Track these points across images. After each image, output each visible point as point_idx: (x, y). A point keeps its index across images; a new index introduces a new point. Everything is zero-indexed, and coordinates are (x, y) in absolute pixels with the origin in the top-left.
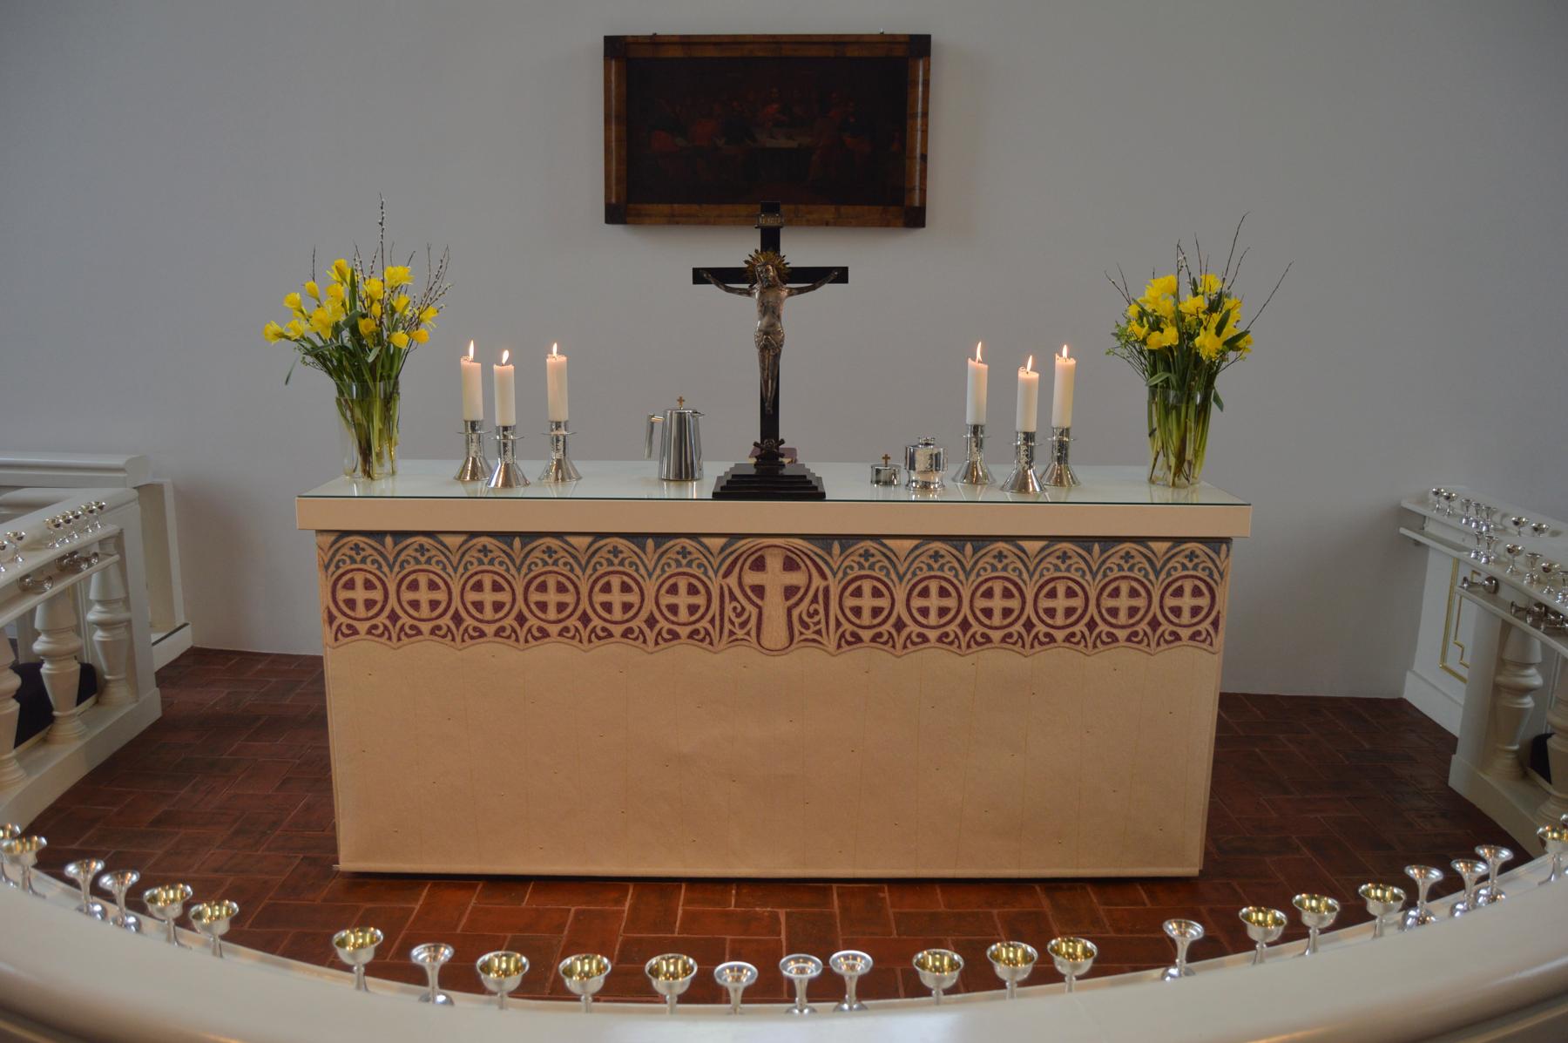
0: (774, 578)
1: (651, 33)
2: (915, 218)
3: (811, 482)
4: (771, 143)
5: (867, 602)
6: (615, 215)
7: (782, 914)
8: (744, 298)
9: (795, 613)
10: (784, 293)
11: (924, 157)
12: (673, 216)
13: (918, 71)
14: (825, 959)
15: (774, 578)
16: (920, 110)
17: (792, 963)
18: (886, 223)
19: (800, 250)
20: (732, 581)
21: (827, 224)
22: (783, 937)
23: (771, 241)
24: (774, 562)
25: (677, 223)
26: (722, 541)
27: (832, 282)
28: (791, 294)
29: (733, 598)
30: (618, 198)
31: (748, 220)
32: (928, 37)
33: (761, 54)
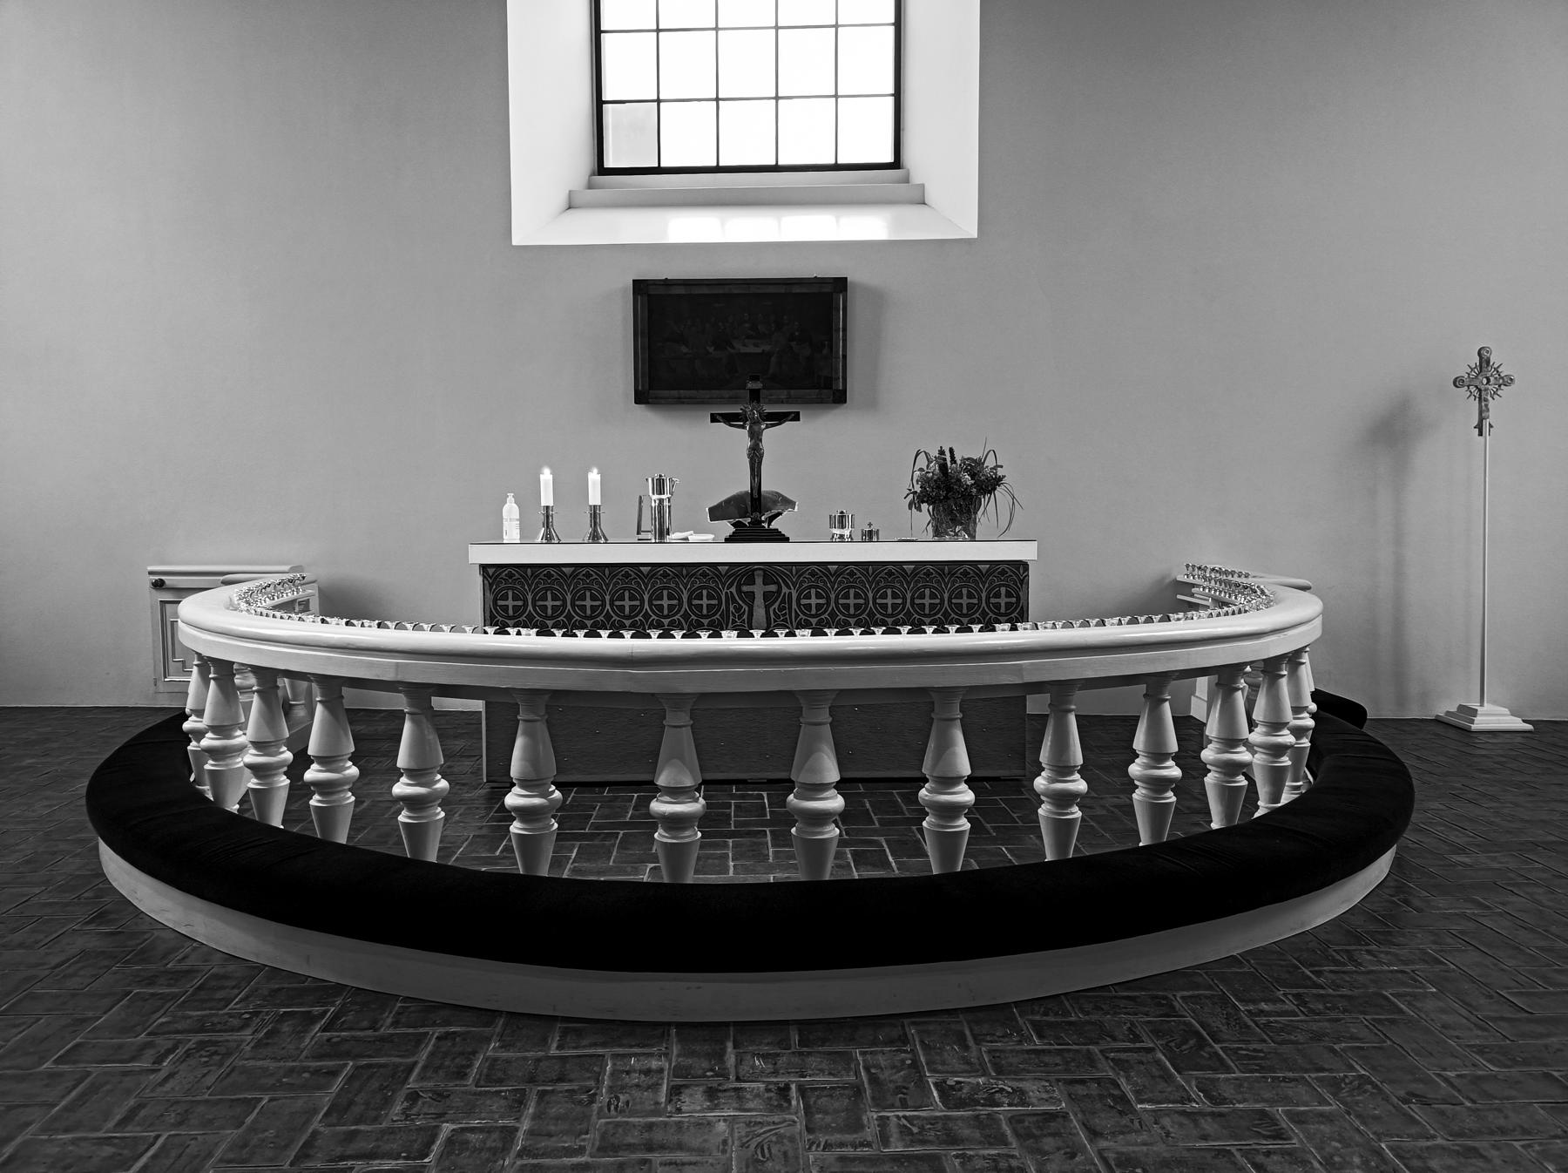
0: (758, 589)
4: (744, 350)
6: (640, 398)
7: (765, 794)
9: (771, 609)
10: (763, 427)
11: (845, 357)
12: (679, 398)
15: (758, 589)
16: (841, 326)
20: (733, 590)
21: (782, 402)
22: (766, 801)
24: (759, 580)
25: (683, 403)
27: (791, 420)
28: (767, 427)
29: (734, 601)
30: (643, 386)
32: (846, 278)
33: (736, 292)
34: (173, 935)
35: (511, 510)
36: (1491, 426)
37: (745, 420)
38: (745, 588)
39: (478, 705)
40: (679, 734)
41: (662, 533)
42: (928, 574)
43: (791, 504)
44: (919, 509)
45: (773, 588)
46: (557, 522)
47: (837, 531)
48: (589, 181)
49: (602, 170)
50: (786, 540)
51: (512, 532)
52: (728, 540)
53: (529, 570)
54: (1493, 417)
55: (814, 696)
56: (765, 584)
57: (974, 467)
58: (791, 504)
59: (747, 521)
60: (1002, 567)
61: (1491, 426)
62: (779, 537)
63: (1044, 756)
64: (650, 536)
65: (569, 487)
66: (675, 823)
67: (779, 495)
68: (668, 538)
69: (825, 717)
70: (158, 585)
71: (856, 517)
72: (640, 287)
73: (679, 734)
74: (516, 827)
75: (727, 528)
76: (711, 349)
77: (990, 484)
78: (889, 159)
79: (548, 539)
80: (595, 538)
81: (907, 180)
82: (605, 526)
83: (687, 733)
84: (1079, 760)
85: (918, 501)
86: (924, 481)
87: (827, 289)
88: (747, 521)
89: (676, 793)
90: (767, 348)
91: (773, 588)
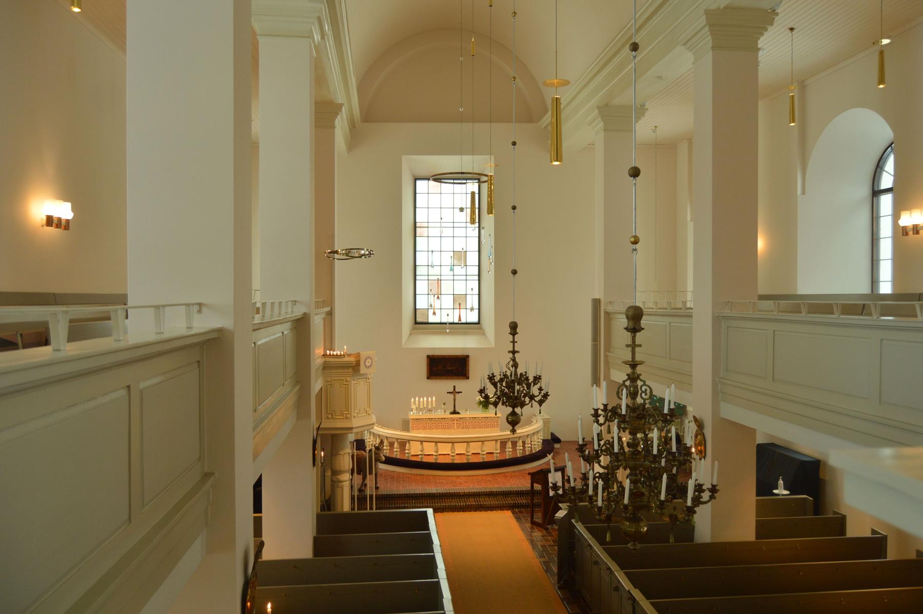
0: (455, 422)
2: (468, 378)
3: (686, 444)
4: (448, 368)
5: (464, 424)
6: (428, 378)
14: (513, 409)
15: (455, 422)
49: (416, 323)
72: (428, 356)
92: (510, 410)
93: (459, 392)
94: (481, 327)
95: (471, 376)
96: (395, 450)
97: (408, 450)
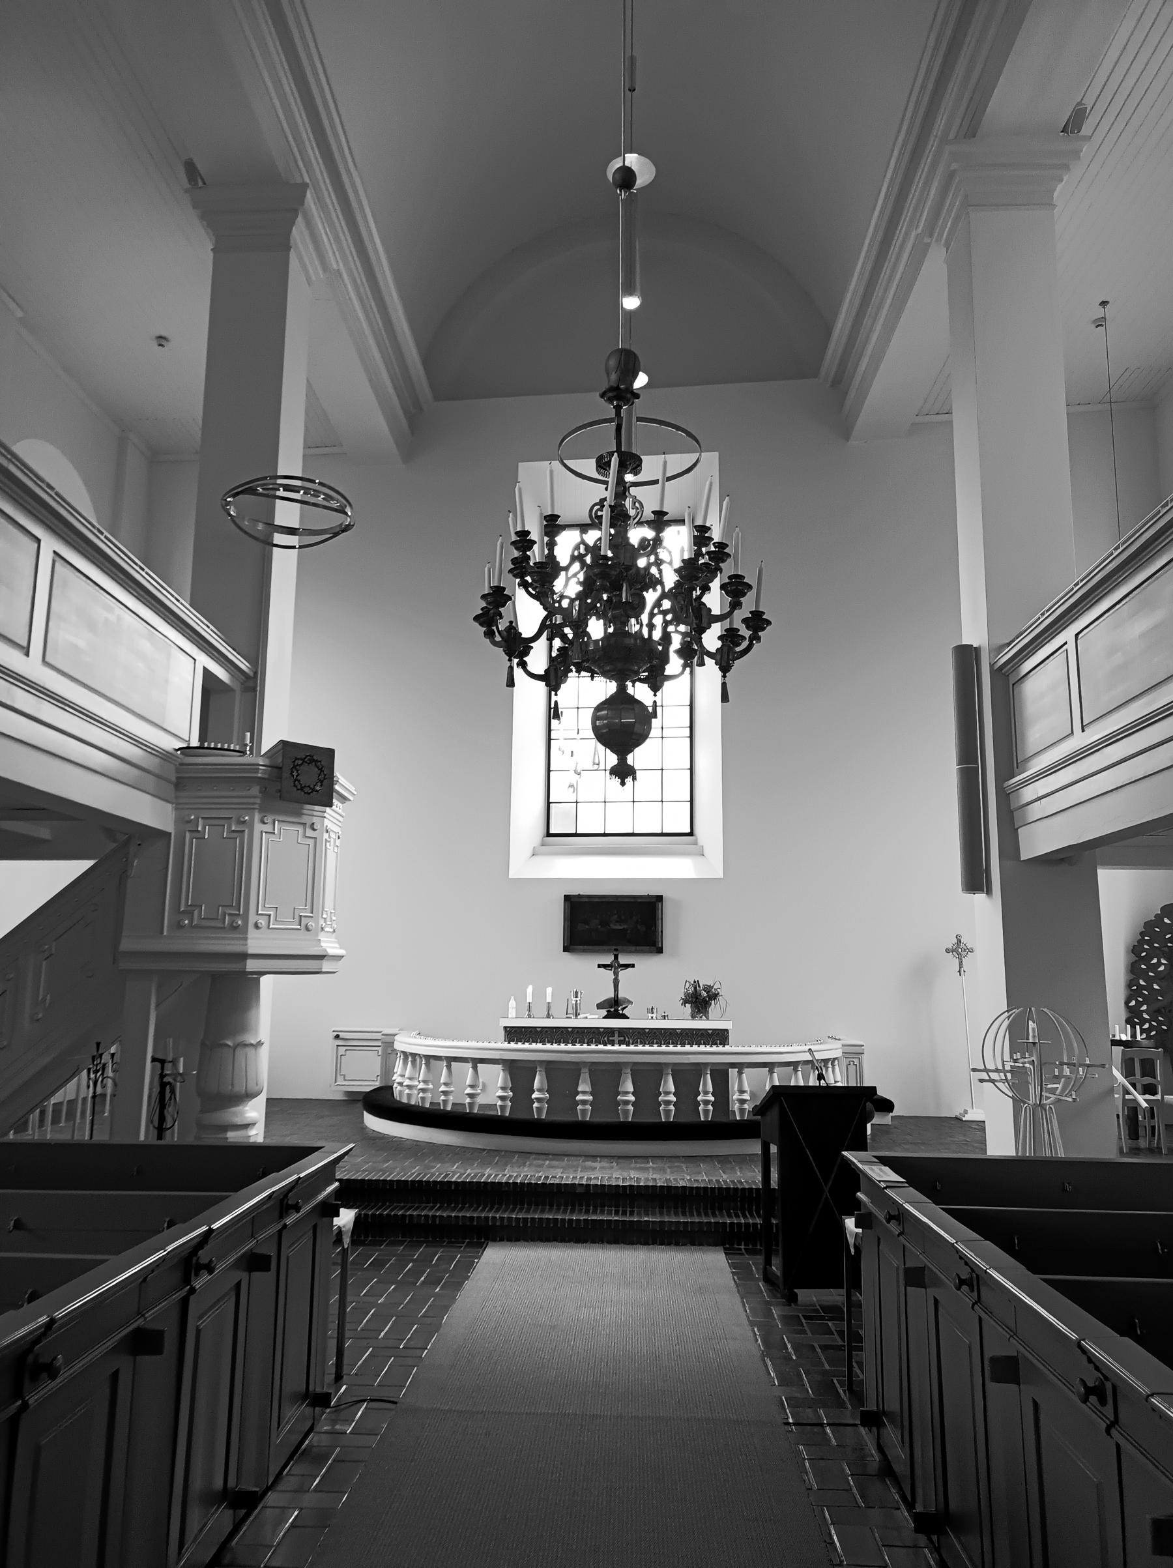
1: (577, 894)
2: (660, 951)
6: (566, 949)
8: (610, 971)
11: (662, 932)
13: (171, 880)
17: (258, 788)
18: (651, 952)
19: (623, 960)
20: (606, 1039)
23: (616, 957)
24: (616, 1035)
26: (603, 1030)
28: (621, 970)
31: (609, 951)
32: (662, 896)
34: (425, 1144)
35: (512, 1003)
36: (964, 971)
37: (612, 967)
38: (611, 1038)
39: (660, 946)
40: (585, 1076)
41: (577, 1015)
42: (687, 1034)
43: (632, 1003)
44: (685, 1006)
45: (622, 1038)
46: (532, 1009)
47: (650, 1015)
48: (543, 840)
49: (549, 835)
50: (628, 1018)
51: (512, 1013)
52: (604, 1018)
53: (523, 1030)
54: (965, 967)
55: (626, 1064)
56: (619, 1037)
57: (708, 989)
58: (632, 1003)
59: (612, 1010)
60: (702, 1031)
61: (964, 971)
62: (625, 1017)
63: (701, 1089)
64: (571, 1016)
65: (539, 993)
66: (584, 1102)
67: (626, 999)
68: (579, 1017)
69: (629, 1071)
70: (337, 1037)
71: (658, 1010)
72: (567, 898)
73: (585, 1076)
74: (536, 1105)
75: (604, 1012)
76: (599, 927)
77: (715, 996)
78: (688, 831)
79: (529, 1016)
80: (548, 1016)
81: (696, 843)
82: (533, 1011)
83: (587, 1075)
84: (711, 1090)
85: (685, 1002)
86: (686, 994)
87: (654, 900)
88: (612, 1010)
89: (584, 1093)
90: (625, 926)
91: (622, 1038)
92: (611, 687)
93: (627, 966)
94: (696, 840)
95: (667, 943)
96: (535, 1095)
97: (445, 1084)
